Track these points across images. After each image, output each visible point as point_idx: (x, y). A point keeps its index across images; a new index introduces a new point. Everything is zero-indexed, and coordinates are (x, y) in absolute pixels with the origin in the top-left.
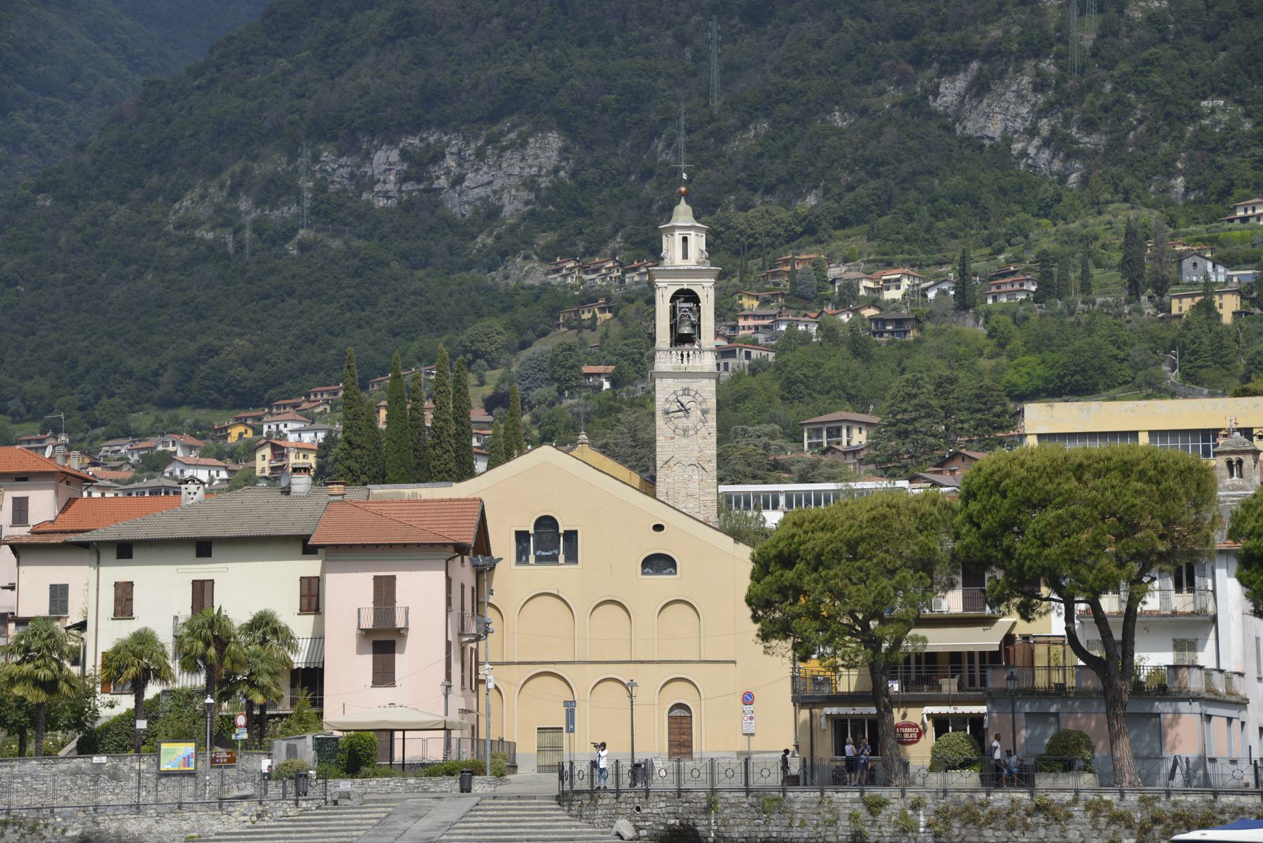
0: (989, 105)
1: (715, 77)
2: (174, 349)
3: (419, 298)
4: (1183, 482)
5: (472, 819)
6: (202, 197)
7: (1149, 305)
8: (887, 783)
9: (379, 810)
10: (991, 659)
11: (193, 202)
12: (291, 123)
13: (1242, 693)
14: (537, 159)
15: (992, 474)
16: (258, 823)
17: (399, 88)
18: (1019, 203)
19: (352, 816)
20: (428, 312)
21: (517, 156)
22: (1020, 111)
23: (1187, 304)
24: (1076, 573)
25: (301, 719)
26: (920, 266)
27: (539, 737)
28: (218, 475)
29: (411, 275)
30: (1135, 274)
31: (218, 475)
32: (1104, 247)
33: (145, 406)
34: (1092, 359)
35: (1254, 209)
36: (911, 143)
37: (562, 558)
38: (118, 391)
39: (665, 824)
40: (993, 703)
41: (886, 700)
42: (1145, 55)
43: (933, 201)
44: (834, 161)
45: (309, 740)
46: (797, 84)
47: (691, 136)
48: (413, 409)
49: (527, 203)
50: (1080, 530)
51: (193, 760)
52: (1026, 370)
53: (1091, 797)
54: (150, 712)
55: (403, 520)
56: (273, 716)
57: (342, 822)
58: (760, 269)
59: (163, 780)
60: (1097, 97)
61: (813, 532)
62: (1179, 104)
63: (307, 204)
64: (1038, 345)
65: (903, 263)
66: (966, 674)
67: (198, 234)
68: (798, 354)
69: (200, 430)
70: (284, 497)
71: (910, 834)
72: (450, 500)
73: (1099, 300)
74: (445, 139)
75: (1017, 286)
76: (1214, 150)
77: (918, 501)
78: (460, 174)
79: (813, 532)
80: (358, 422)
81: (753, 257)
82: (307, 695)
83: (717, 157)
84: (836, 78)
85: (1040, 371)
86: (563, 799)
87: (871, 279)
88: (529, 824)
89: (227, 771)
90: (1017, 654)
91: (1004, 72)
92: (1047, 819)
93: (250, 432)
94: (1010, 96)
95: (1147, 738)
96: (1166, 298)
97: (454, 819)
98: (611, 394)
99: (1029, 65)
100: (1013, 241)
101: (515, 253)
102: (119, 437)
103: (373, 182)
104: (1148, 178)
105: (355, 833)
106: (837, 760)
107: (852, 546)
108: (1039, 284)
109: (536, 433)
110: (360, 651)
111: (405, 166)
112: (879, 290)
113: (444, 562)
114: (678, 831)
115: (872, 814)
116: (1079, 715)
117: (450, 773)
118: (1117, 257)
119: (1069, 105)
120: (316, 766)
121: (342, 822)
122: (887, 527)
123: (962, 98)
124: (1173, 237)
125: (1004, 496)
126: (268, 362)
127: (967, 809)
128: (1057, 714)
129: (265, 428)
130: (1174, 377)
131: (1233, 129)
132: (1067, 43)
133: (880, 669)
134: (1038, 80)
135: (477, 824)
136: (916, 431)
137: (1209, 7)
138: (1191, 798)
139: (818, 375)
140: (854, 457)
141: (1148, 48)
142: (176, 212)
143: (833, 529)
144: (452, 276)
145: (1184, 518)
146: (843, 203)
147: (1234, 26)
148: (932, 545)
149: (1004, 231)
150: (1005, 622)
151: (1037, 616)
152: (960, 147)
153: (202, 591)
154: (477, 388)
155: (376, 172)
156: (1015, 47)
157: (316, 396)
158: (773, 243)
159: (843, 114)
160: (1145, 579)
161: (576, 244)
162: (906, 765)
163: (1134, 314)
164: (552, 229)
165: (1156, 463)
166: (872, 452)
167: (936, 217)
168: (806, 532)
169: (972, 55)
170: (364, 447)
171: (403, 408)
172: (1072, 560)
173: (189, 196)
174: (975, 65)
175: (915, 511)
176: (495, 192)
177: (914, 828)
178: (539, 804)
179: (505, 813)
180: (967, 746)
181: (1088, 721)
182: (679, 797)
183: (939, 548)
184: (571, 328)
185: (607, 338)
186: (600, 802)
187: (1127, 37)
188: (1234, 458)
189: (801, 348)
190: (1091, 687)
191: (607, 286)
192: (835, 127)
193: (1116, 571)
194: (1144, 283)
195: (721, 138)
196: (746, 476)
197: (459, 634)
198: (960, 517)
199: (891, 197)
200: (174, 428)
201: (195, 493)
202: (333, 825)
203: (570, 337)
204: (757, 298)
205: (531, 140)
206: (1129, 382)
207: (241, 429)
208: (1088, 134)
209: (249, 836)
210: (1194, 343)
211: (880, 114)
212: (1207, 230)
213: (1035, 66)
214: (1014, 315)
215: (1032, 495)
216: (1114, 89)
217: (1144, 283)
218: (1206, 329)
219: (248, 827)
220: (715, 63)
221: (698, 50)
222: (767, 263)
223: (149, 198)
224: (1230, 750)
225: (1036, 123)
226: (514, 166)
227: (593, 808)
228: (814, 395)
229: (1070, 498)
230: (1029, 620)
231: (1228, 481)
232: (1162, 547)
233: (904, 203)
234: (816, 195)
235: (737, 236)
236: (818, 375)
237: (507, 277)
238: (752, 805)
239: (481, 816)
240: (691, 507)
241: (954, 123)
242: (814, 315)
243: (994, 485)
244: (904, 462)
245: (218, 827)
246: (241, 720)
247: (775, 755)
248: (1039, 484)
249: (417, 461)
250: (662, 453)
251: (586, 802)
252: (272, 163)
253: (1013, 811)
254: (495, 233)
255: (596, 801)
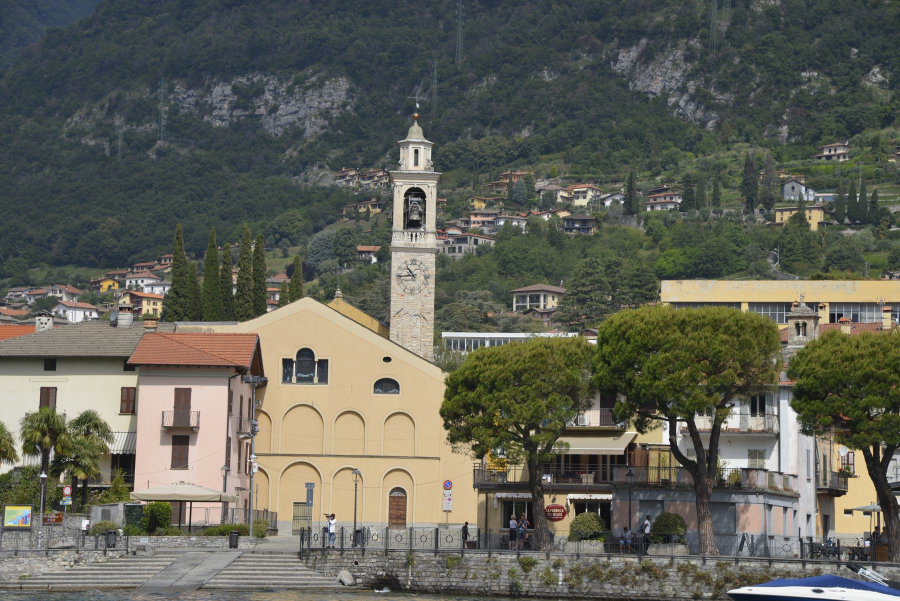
0: (653, 70)
1: (460, 43)
2: (63, 223)
3: (242, 193)
4: (756, 335)
5: (235, 568)
6: (88, 115)
7: (760, 215)
8: (538, 549)
9: (166, 559)
10: (619, 460)
11: (81, 118)
12: (154, 64)
13: (795, 489)
14: (330, 96)
15: (620, 326)
16: (75, 567)
17: (233, 41)
18: (672, 140)
19: (146, 563)
20: (249, 204)
21: (317, 94)
22: (675, 75)
23: (787, 215)
24: (678, 399)
25: (117, 491)
26: (601, 183)
27: (294, 509)
28: (91, 315)
29: (238, 176)
30: (751, 193)
31: (91, 315)
32: (730, 173)
33: (41, 263)
34: (718, 252)
35: (835, 150)
36: (597, 95)
37: (316, 379)
38: (21, 252)
39: (375, 575)
40: (617, 492)
41: (539, 488)
42: (764, 38)
43: (612, 137)
44: (543, 105)
45: (121, 506)
46: (518, 49)
47: (442, 84)
48: (224, 270)
49: (322, 128)
50: (682, 369)
51: (29, 519)
52: (672, 259)
53: (682, 562)
54: (5, 483)
55: (199, 348)
56: (94, 489)
57: (138, 568)
58: (487, 181)
59: (6, 534)
60: (729, 67)
61: (490, 365)
62: (785, 74)
63: (164, 122)
64: (682, 241)
65: (589, 180)
66: (600, 471)
67: (83, 141)
68: (511, 242)
69: (80, 282)
70: (112, 329)
71: (552, 586)
72: (235, 334)
73: (725, 211)
74: (265, 79)
75: (668, 199)
76: (809, 108)
77: (567, 344)
78: (275, 105)
79: (490, 365)
80: (183, 278)
81: (483, 172)
82: (122, 474)
83: (460, 100)
84: (545, 46)
85: (682, 259)
86: (303, 554)
87: (566, 191)
88: (276, 572)
89: (55, 528)
90: (636, 458)
91: (664, 46)
92: (650, 577)
93: (117, 285)
94: (668, 64)
95: (726, 521)
96: (772, 211)
97: (221, 568)
98: (377, 267)
99: (682, 42)
100: (667, 167)
101: (313, 163)
102: (21, 285)
103: (212, 108)
104: (763, 126)
105: (146, 576)
106: (504, 531)
107: (518, 375)
108: (684, 198)
109: (322, 292)
110: (163, 443)
111: (236, 97)
112: (571, 199)
113: (227, 380)
114: (384, 580)
115: (525, 570)
116: (678, 503)
117: (222, 533)
118: (739, 181)
119: (710, 72)
120: (124, 526)
121: (138, 568)
122: (543, 362)
123: (634, 64)
124: (778, 168)
125: (628, 342)
126: (131, 235)
127: (593, 568)
128: (662, 502)
129: (128, 283)
130: (775, 267)
131: (823, 93)
132: (709, 28)
133: (536, 466)
134: (688, 53)
135: (237, 572)
136: (591, 299)
137: (809, 6)
138: (753, 565)
139: (525, 258)
140: (548, 317)
141: (766, 33)
142: (68, 125)
143: (505, 362)
144: (267, 178)
145: (756, 362)
146: (547, 136)
147: (826, 20)
148: (575, 377)
149: (661, 160)
150: (632, 432)
151: (648, 430)
152: (632, 99)
153: (48, 396)
154: (282, 259)
155: (214, 101)
156: (672, 29)
157: (165, 261)
158: (498, 163)
159: (550, 72)
160: (727, 405)
161: (357, 159)
162: (552, 536)
163: (749, 221)
164: (340, 147)
165: (737, 321)
166: (560, 313)
167: (613, 148)
168: (485, 364)
169: (641, 34)
170: (187, 297)
171: (216, 269)
172: (675, 390)
173: (78, 114)
174: (644, 41)
175: (564, 351)
176: (300, 119)
177: (555, 581)
178: (285, 558)
179: (259, 564)
180: (596, 523)
181: (683, 507)
182: (386, 555)
183: (580, 379)
184: (351, 218)
185: (377, 226)
186: (329, 557)
187: (751, 25)
188: (800, 321)
189: (514, 238)
190: (688, 482)
191: (378, 189)
192: (544, 81)
193: (706, 399)
194: (757, 200)
195: (463, 87)
196: (465, 327)
197: (237, 433)
198: (596, 356)
199: (582, 133)
200: (62, 280)
201: (46, 324)
202: (130, 570)
203: (350, 225)
204: (484, 201)
205: (327, 83)
206: (744, 270)
207: (110, 283)
208: (722, 93)
209: (66, 577)
210: (790, 243)
211: (576, 73)
212: (803, 164)
213: (687, 43)
214: (665, 219)
215: (648, 342)
216: (741, 62)
217: (757, 200)
218: (799, 234)
219: (67, 570)
220: (460, 33)
221: (449, 23)
222: (493, 177)
223: (49, 114)
224: (785, 530)
225: (686, 84)
226: (314, 101)
227: (323, 561)
228: (522, 271)
229: (675, 345)
230: (643, 433)
231: (796, 338)
232: (740, 382)
233: (591, 137)
234: (529, 129)
235: (472, 157)
236: (525, 258)
237: (306, 181)
238: (439, 563)
239: (241, 565)
240: (414, 345)
241: (628, 82)
242: (524, 215)
243: (621, 334)
244: (582, 321)
245: (44, 569)
246: (67, 491)
247: (458, 527)
248: (653, 334)
249: (225, 308)
250: (394, 308)
251: (319, 557)
252: (140, 92)
253: (626, 571)
254: (299, 149)
255: (326, 557)
